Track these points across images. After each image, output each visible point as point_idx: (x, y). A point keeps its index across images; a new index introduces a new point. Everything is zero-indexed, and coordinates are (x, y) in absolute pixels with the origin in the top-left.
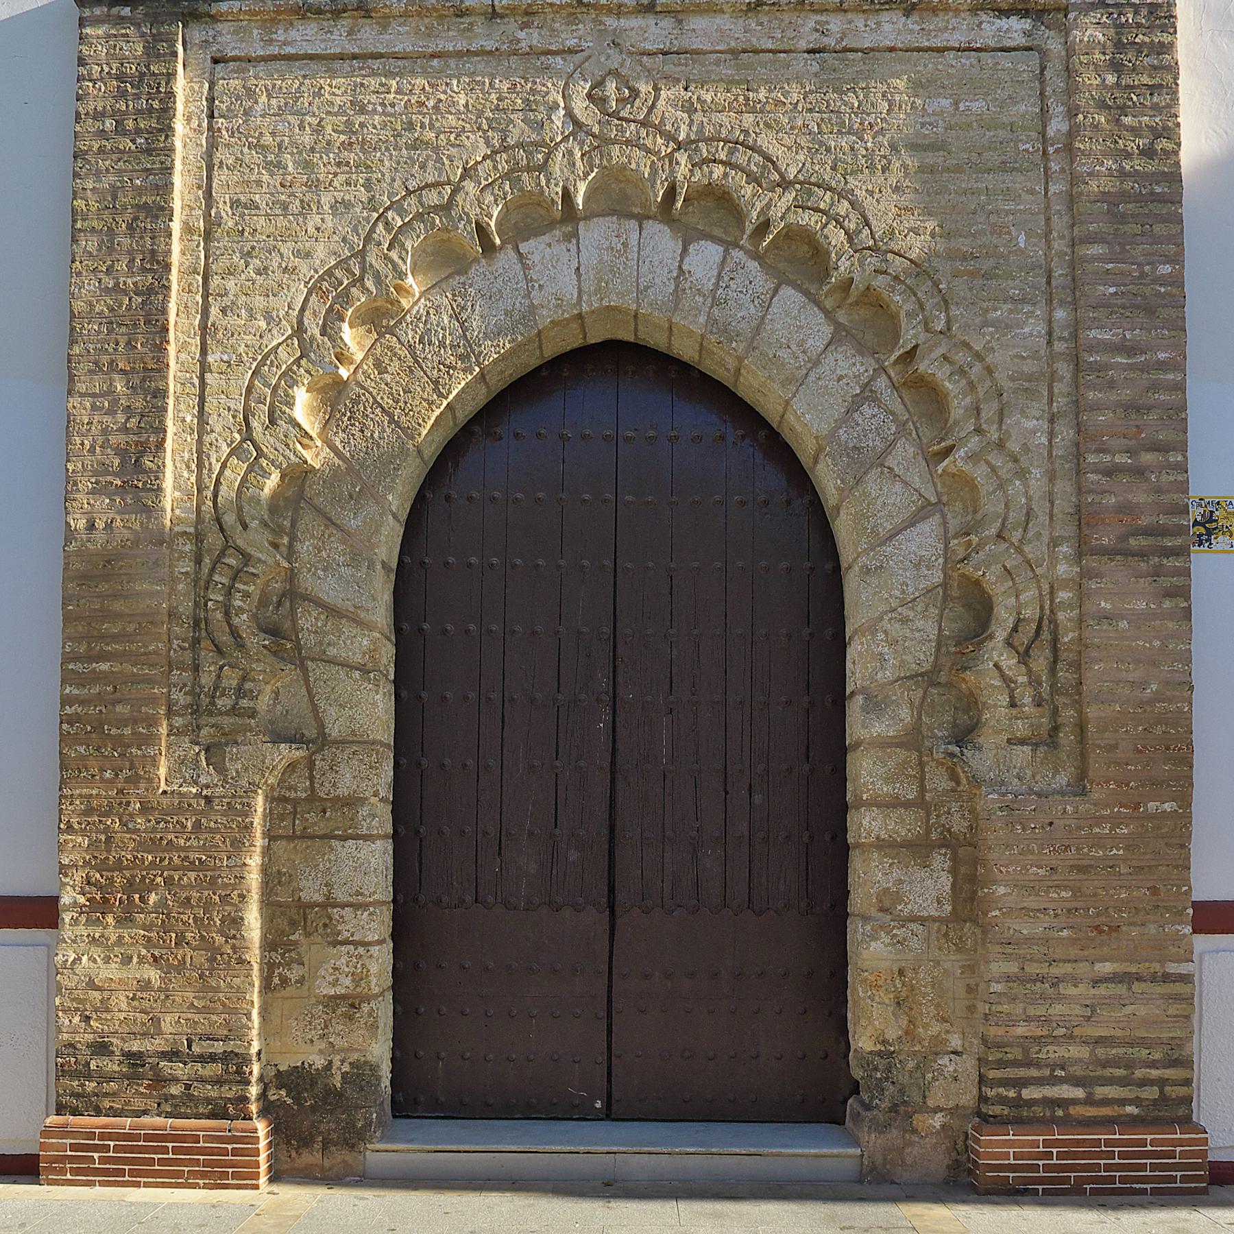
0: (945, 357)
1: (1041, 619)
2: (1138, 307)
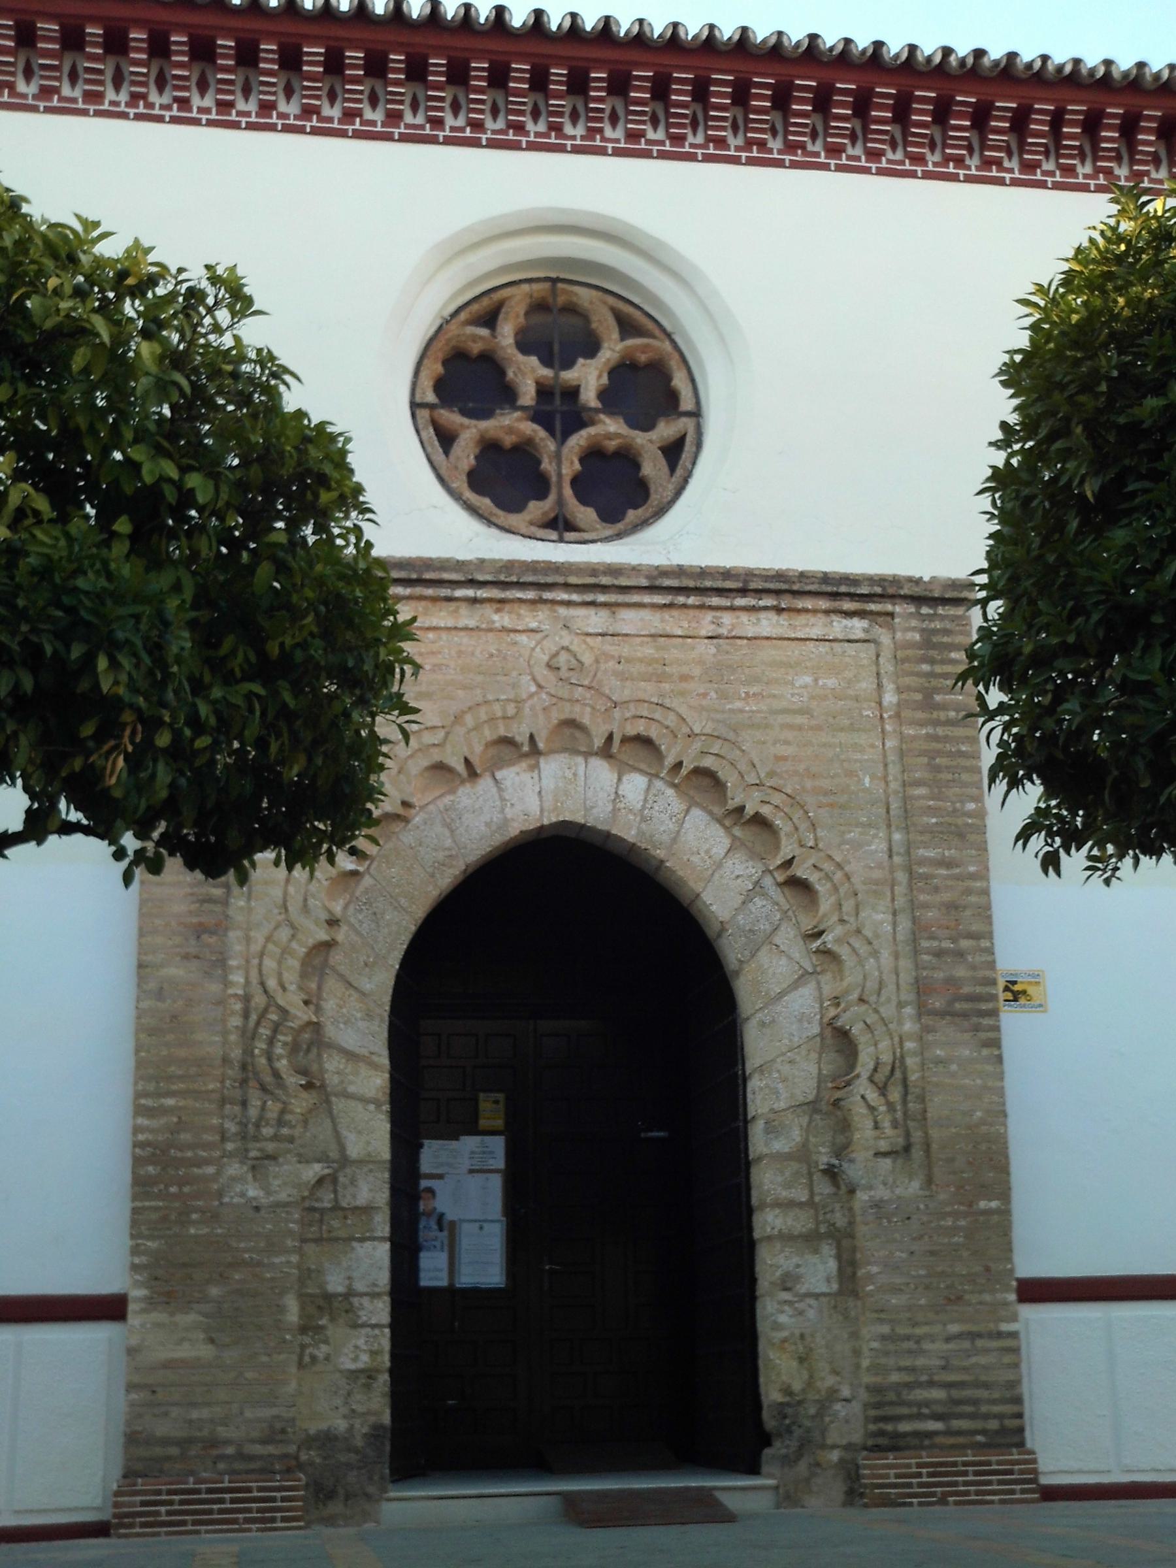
1: (894, 1062)
2: (952, 833)
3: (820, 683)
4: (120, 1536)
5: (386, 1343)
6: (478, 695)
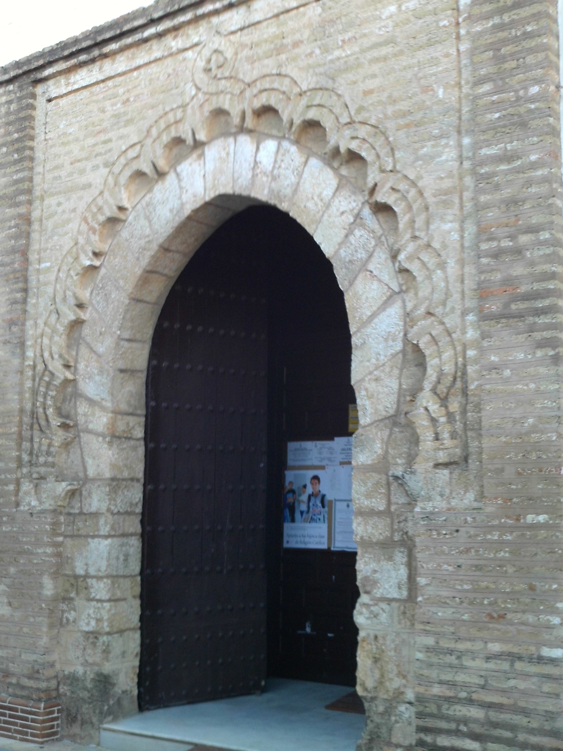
0: (393, 189)
1: (456, 372)
2: (513, 124)
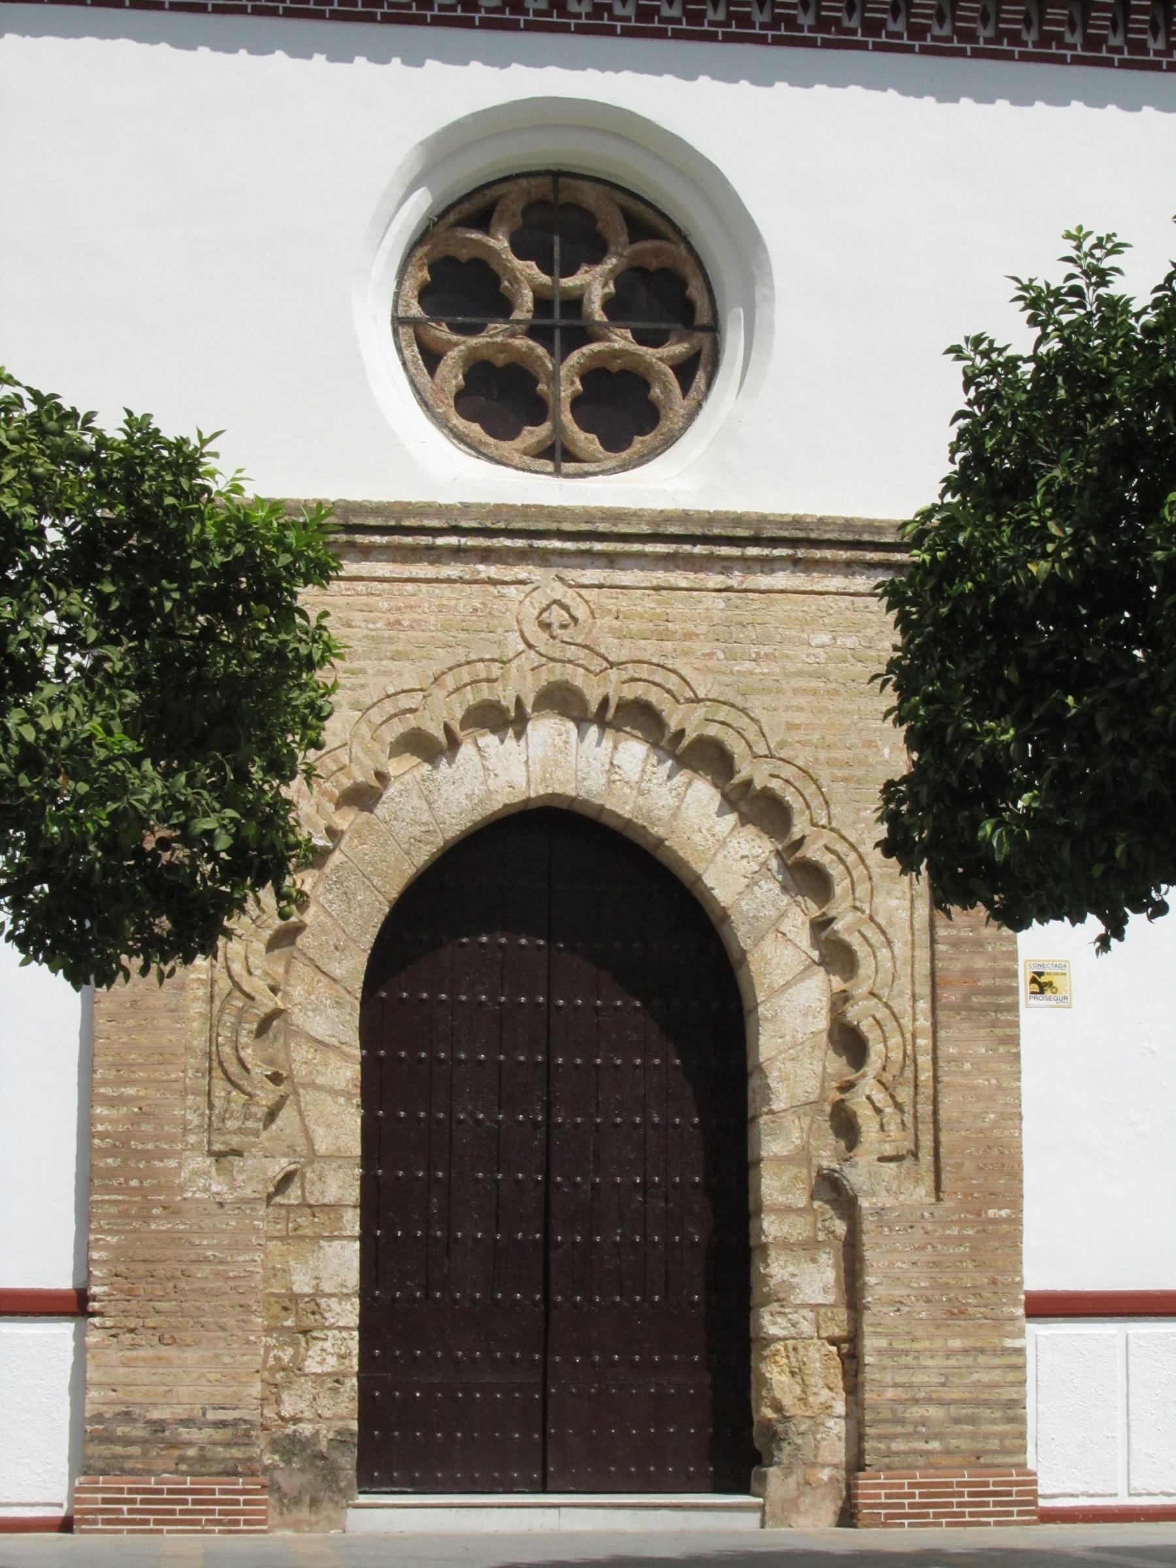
0: (827, 848)
3: (839, 642)
4: (83, 1531)
5: (354, 1346)
6: (461, 655)
